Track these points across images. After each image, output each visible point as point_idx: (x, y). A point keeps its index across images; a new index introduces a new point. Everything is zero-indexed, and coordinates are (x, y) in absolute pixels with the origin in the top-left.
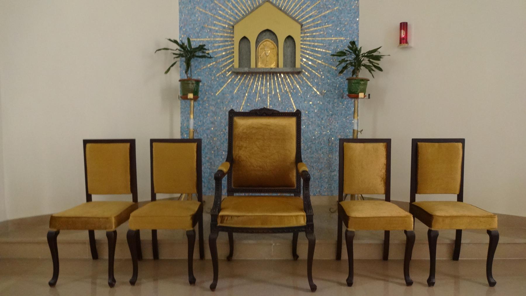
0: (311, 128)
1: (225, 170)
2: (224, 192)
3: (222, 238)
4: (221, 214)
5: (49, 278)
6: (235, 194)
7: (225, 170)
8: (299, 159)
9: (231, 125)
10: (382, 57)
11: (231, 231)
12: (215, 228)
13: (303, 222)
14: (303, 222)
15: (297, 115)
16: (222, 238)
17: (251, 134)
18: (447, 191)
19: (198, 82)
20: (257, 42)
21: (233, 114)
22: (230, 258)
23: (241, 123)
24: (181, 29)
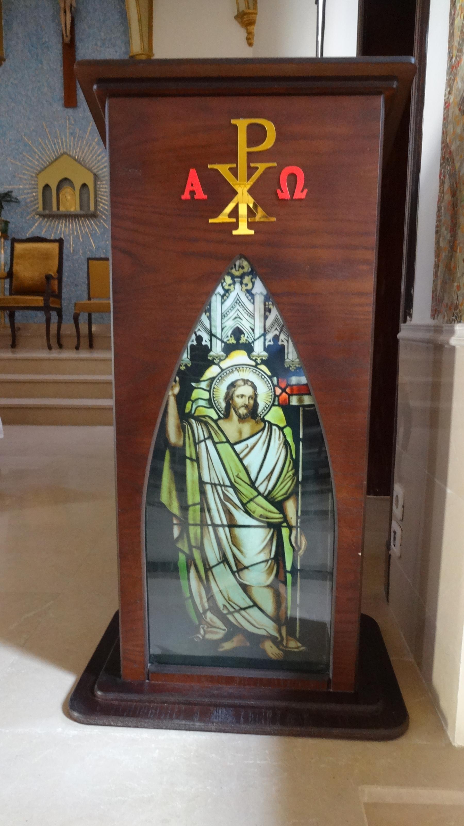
15: (60, 242)
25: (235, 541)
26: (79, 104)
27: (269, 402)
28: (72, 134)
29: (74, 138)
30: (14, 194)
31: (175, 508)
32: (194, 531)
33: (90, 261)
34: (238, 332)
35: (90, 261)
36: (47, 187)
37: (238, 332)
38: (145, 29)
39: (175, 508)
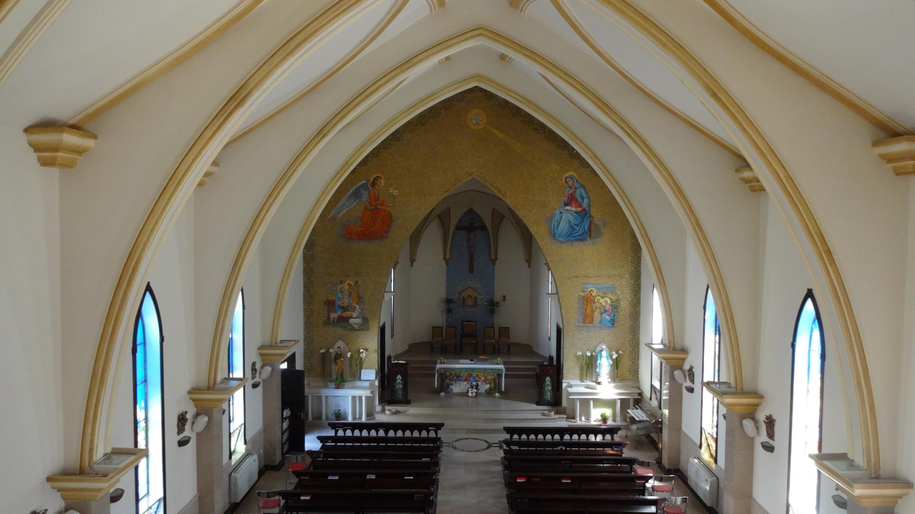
9: (462, 324)
15: (476, 321)
20: (467, 298)
21: (463, 321)
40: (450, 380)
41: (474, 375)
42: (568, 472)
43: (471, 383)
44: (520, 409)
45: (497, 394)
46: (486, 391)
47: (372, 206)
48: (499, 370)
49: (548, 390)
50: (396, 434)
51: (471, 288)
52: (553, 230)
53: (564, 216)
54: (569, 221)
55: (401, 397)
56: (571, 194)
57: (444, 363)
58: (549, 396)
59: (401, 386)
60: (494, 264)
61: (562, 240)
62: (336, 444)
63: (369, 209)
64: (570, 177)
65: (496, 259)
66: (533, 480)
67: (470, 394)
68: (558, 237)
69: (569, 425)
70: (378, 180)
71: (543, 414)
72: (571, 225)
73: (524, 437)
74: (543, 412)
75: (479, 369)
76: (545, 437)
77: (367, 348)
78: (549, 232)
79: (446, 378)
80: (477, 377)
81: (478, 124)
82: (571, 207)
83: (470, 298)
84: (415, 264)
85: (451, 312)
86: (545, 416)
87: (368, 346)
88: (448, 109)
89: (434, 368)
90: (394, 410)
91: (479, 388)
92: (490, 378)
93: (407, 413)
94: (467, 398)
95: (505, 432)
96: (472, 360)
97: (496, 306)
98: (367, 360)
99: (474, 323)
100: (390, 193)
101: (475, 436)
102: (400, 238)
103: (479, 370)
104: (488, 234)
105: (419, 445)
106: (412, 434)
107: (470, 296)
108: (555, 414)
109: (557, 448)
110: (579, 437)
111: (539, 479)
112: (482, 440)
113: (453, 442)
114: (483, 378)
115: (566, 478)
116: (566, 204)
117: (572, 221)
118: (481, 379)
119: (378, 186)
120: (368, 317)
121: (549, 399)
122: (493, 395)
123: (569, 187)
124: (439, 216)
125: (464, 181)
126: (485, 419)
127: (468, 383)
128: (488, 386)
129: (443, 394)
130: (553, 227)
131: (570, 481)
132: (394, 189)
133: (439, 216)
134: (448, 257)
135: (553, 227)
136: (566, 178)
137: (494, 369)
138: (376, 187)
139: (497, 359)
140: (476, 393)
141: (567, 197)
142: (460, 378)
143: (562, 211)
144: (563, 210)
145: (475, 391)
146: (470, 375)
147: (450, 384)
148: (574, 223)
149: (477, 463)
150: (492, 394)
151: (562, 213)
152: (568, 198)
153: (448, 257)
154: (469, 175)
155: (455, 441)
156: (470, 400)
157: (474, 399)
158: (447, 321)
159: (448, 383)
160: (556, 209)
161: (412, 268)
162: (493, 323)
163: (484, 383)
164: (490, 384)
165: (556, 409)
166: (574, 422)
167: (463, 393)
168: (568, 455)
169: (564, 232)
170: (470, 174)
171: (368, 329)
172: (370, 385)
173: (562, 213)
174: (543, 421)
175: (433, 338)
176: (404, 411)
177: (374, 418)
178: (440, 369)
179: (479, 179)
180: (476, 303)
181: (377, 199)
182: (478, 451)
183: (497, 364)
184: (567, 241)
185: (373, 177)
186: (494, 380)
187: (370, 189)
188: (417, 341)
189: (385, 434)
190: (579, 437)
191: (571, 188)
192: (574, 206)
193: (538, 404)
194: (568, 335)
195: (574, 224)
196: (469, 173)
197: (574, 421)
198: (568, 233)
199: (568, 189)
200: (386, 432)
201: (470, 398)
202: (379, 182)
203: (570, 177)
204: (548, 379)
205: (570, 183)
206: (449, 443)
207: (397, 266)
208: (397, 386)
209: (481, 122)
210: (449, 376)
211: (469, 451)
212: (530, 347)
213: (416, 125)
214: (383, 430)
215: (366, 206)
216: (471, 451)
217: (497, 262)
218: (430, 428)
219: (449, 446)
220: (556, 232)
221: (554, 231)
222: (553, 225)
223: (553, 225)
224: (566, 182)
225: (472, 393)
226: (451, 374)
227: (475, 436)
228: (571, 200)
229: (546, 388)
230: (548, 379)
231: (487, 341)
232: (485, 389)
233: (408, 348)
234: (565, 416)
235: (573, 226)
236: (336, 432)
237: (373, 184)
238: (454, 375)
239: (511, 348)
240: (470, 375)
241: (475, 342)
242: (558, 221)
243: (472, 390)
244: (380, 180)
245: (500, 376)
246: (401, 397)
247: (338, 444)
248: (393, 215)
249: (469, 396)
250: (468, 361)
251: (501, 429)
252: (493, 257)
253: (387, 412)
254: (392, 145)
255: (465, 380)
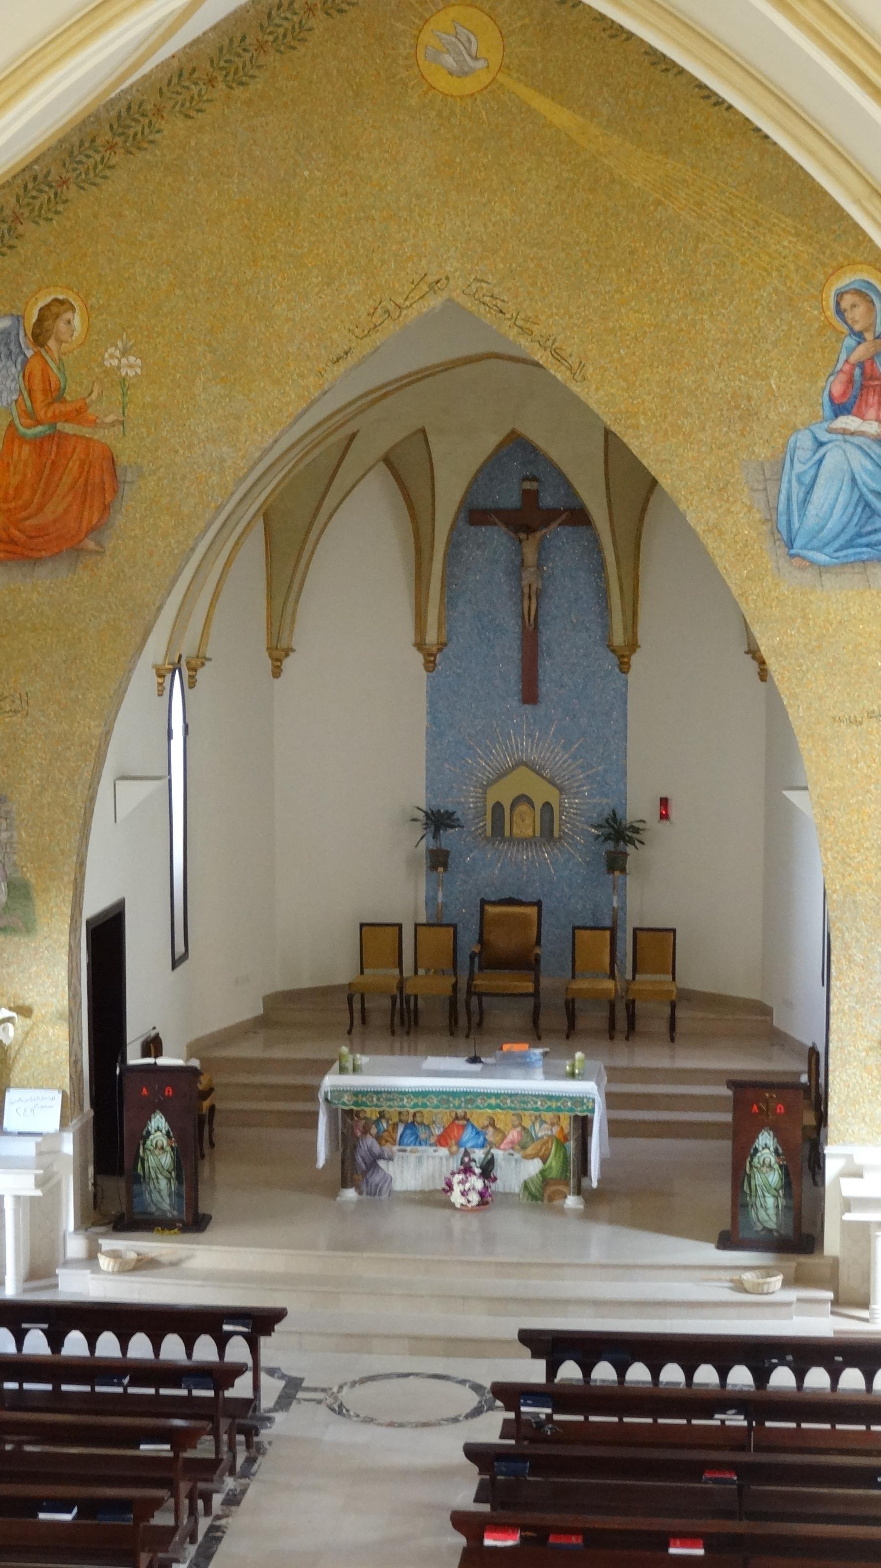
0: (573, 900)
1: (477, 951)
2: (476, 970)
3: (474, 1000)
4: (474, 983)
5: (348, 1028)
6: (506, 1047)
7: (477, 951)
8: (538, 942)
9: (482, 911)
10: (637, 843)
11: (480, 995)
12: (470, 992)
13: (531, 990)
14: (531, 990)
15: (539, 904)
16: (474, 1000)
17: (501, 920)
18: (663, 972)
19: (447, 853)
20: (513, 806)
21: (484, 902)
22: (480, 1024)
23: (491, 910)
24: (427, 788)
25: (765, 1201)
26: (540, 699)
27: (816, 438)
28: (529, 735)
29: (532, 742)
30: (458, 815)
31: (748, 1191)
32: (753, 1198)
33: (576, 931)
34: (766, 1145)
35: (576, 931)
36: (498, 806)
37: (766, 1145)
38: (629, 613)
39: (748, 1191)
40: (378, 1138)
41: (479, 1117)
42: (729, 1515)
43: (466, 1153)
44: (648, 1261)
45: (572, 1202)
46: (526, 1186)
47: (39, 423)
48: (578, 1101)
49: (767, 1186)
50: (124, 1348)
51: (525, 764)
52: (783, 520)
53: (833, 458)
54: (854, 480)
55: (166, 1205)
56: (861, 365)
57: (356, 1070)
58: (772, 1211)
59: (166, 1160)
60: (624, 666)
61: (821, 558)
62: (56, 1388)
63: (23, 439)
64: (858, 292)
65: (633, 645)
66: (552, 1540)
67: (456, 1198)
68: (804, 547)
69: (835, 1332)
70: (57, 316)
71: (740, 1287)
72: (861, 496)
73: (638, 1373)
74: (735, 1275)
75: (497, 1096)
76: (723, 1374)
77: (28, 1002)
78: (765, 528)
79: (366, 1131)
80: (491, 1130)
81: (463, 73)
82: (862, 416)
83: (523, 808)
84: (288, 664)
85: (445, 865)
86: (746, 1291)
87: (30, 998)
88: (341, 11)
89: (311, 1093)
90: (132, 1256)
91: (497, 1172)
92: (542, 1131)
93: (185, 1265)
94: (448, 1212)
95: (527, 1351)
96: (474, 1060)
97: (631, 841)
98: (27, 1051)
99: (532, 911)
100: (107, 372)
101: (439, 1365)
102: (151, 554)
103: (493, 1101)
104: (596, 540)
105: (793, 1425)
106: (157, 1348)
107: (523, 799)
108: (786, 1284)
109: (711, 1417)
110: (835, 1380)
111: (576, 1540)
112: (463, 1382)
113: (341, 1388)
114: (513, 1135)
115: (688, 1538)
116: (839, 409)
117: (869, 481)
118: (504, 1136)
119: (60, 342)
120: (33, 881)
121: (772, 1224)
122: (557, 1202)
123: (853, 332)
124: (387, 460)
125: (411, 314)
126: (499, 1300)
127: (452, 1154)
128: (534, 1167)
129: (350, 1194)
130: (782, 507)
131: (700, 1552)
132: (124, 353)
133: (387, 460)
134: (432, 637)
135: (782, 507)
136: (840, 295)
137: (558, 1098)
138: (52, 343)
139: (573, 1057)
140: (482, 1194)
141: (843, 378)
142: (422, 1133)
143: (824, 437)
144: (830, 431)
145: (479, 1184)
146: (460, 1121)
147: (381, 1157)
148: (874, 485)
149: (406, 1474)
150: (551, 1199)
151: (821, 444)
152: (850, 381)
153: (432, 637)
154: (431, 287)
155: (354, 1384)
156: (458, 1223)
157: (474, 1222)
158: (430, 901)
159: (370, 1150)
160: (795, 430)
161: (277, 681)
162: (623, 907)
163: (517, 1155)
164: (544, 1160)
165: (792, 1262)
166: (866, 1320)
167: (431, 1192)
168: (759, 1449)
169: (833, 524)
170: (434, 287)
171: (28, 928)
172: (40, 1154)
173: (821, 444)
174: (732, 1311)
175: (362, 972)
176: (174, 1258)
177: (56, 1286)
178: (338, 1092)
179: (469, 304)
180: (547, 834)
181: (56, 395)
182: (425, 1425)
183: (572, 1075)
184: (843, 565)
185: (41, 304)
186: (561, 1142)
187: (29, 353)
188: (305, 983)
189: (50, 1344)
190: (835, 1380)
191: (860, 336)
192: (872, 413)
193: (726, 1242)
194: (850, 961)
195: (873, 492)
196: (431, 279)
197: (864, 1314)
198: (851, 530)
199: (850, 341)
200: (56, 1340)
201: (458, 1215)
202: (61, 325)
203: (858, 292)
204: (158, 1122)
205: (858, 315)
206: (323, 1390)
207: (201, 674)
208: (151, 1161)
209: (481, 64)
210: (377, 1122)
211: (391, 1424)
212: (764, 1010)
213: (211, 82)
214: (43, 1330)
215: (11, 425)
216: (401, 1425)
217: (635, 659)
218: (227, 1328)
219: (319, 1402)
220: (796, 524)
221: (789, 522)
222: (783, 497)
223: (783, 497)
224: (840, 312)
225: (464, 1193)
226: (382, 1115)
227: (439, 1365)
228: (862, 387)
229: (758, 1179)
230: (158, 1122)
231: (582, 984)
232: (524, 1176)
233: (259, 1011)
234: (830, 1295)
235: (871, 498)
236: (552, 1371)
237: (40, 336)
238: (396, 1119)
239: (679, 1014)
240: (460, 1121)
241: (529, 987)
242: (807, 479)
243: (462, 1182)
244: (68, 315)
245: (583, 1125)
246: (166, 1205)
247: (65, 1388)
248: (122, 461)
249: (452, 1206)
250: (459, 1063)
251: (508, 1342)
252: (619, 639)
253: (105, 1262)
254: (111, 167)
255: (442, 1141)
